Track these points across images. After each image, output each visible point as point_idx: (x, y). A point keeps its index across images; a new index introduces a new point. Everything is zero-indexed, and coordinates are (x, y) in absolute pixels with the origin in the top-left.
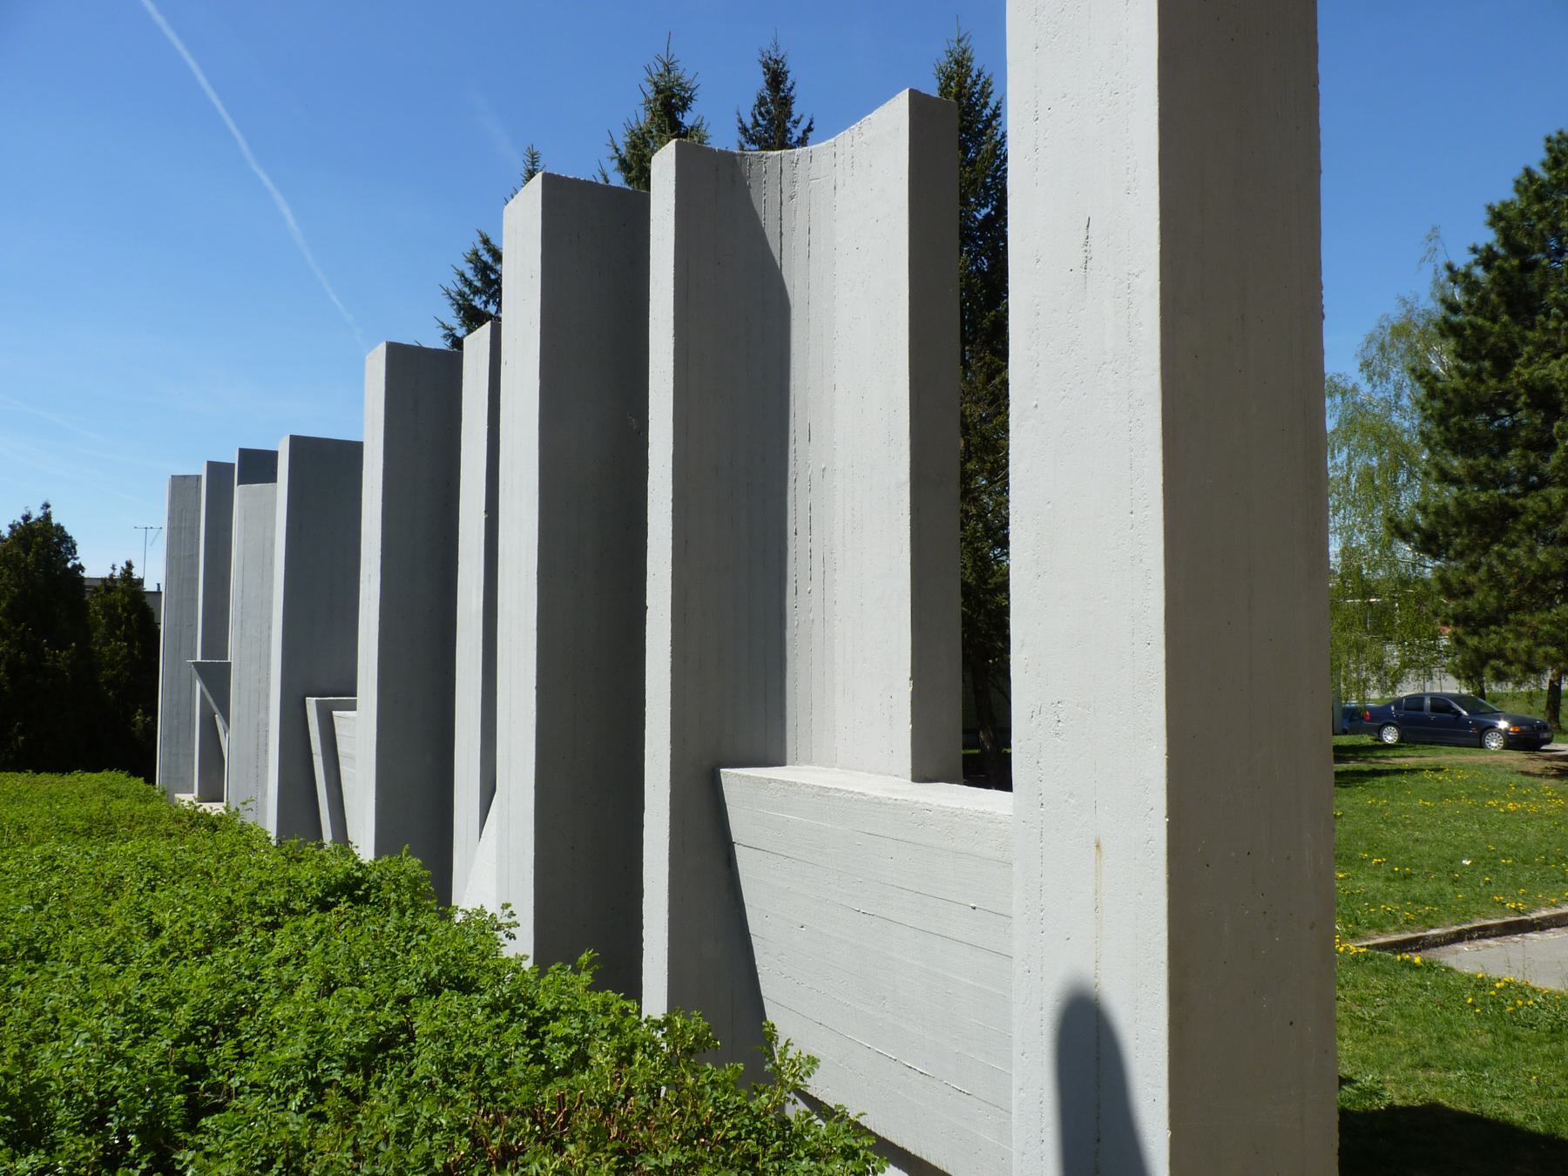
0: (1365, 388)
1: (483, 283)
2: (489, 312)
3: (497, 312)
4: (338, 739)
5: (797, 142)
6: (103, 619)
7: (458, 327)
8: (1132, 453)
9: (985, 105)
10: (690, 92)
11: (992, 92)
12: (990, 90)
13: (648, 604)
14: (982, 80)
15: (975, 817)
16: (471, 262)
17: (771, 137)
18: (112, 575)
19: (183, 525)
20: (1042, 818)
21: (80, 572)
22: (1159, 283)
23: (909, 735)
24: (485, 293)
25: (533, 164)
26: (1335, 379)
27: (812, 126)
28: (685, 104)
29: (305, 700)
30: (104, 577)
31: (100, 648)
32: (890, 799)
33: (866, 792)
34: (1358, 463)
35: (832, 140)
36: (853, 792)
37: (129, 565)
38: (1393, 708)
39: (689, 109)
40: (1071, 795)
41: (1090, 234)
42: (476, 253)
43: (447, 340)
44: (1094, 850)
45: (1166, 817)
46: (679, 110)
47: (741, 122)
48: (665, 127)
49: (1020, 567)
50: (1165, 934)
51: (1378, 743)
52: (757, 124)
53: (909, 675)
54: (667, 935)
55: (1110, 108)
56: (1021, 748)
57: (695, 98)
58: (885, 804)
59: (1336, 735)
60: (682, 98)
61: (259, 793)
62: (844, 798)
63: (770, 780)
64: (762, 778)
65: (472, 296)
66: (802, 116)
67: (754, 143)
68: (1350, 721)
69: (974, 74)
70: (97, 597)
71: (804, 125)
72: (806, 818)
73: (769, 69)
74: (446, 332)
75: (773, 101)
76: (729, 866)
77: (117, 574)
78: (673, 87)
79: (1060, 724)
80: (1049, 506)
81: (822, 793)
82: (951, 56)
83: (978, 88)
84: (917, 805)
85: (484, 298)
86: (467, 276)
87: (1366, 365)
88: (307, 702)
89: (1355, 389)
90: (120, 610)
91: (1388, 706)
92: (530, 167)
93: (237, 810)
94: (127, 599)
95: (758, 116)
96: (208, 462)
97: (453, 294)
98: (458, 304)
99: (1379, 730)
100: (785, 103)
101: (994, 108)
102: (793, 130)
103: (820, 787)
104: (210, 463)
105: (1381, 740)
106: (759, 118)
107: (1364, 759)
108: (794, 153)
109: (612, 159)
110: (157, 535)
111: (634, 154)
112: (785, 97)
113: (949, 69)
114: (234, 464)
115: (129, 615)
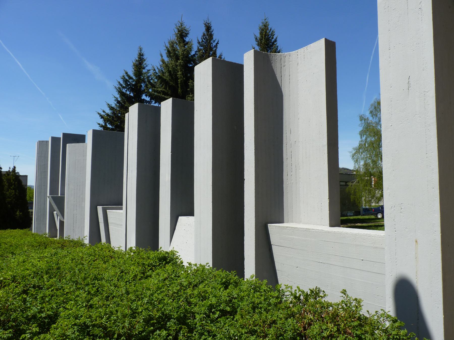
0: (371, 118)
1: (126, 85)
2: (127, 94)
3: (129, 94)
4: (109, 218)
5: (214, 47)
6: (7, 183)
7: (119, 98)
8: (426, 138)
9: (273, 38)
10: (188, 32)
11: (275, 34)
12: (274, 34)
13: (245, 178)
14: (272, 31)
15: (364, 235)
16: (122, 79)
17: (206, 45)
18: (9, 170)
19: (42, 156)
20: (396, 235)
21: (1, 169)
22: (435, 94)
23: (328, 214)
24: (126, 88)
25: (141, 51)
26: (362, 116)
27: (219, 42)
28: (186, 35)
29: (106, 212)
30: (7, 171)
31: (6, 192)
32: (332, 231)
33: (324, 230)
34: (369, 140)
35: (297, 51)
36: (319, 230)
37: (15, 167)
38: (380, 208)
39: (188, 36)
40: (406, 228)
41: (408, 80)
42: (124, 76)
43: (116, 101)
44: (415, 243)
45: (441, 233)
46: (185, 37)
47: (198, 40)
48: (181, 41)
49: (387, 168)
50: (441, 264)
51: (376, 218)
52: (203, 41)
53: (328, 198)
54: (255, 271)
55: (416, 48)
56: (388, 216)
57: (189, 33)
58: (331, 233)
59: (360, 214)
60: (186, 33)
61: (74, 235)
62: (315, 231)
63: (287, 227)
64: (284, 226)
65: (122, 89)
66: (216, 39)
67: (202, 46)
68: (365, 212)
69: (269, 29)
70: (5, 177)
71: (216, 42)
72: (300, 237)
73: (206, 26)
74: (115, 99)
75: (207, 35)
76: (270, 251)
77: (11, 170)
78: (183, 30)
79: (402, 210)
80: (397, 152)
81: (307, 230)
82: (263, 24)
83: (270, 33)
84: (343, 233)
85: (126, 89)
86: (121, 83)
87: (371, 112)
88: (98, 207)
89: (368, 119)
90: (12, 181)
91: (379, 208)
92: (140, 52)
93: (82, 239)
94: (14, 178)
95: (203, 39)
96: (52, 137)
97: (117, 88)
98: (119, 91)
99: (377, 214)
100: (211, 36)
101: (275, 39)
102: (213, 43)
103: (306, 228)
104: (52, 137)
105: (377, 217)
106: (203, 39)
107: (373, 222)
108: (284, 54)
109: (165, 50)
110: (17, 158)
111: (172, 49)
112: (211, 34)
113: (262, 27)
114: (60, 138)
115: (15, 183)
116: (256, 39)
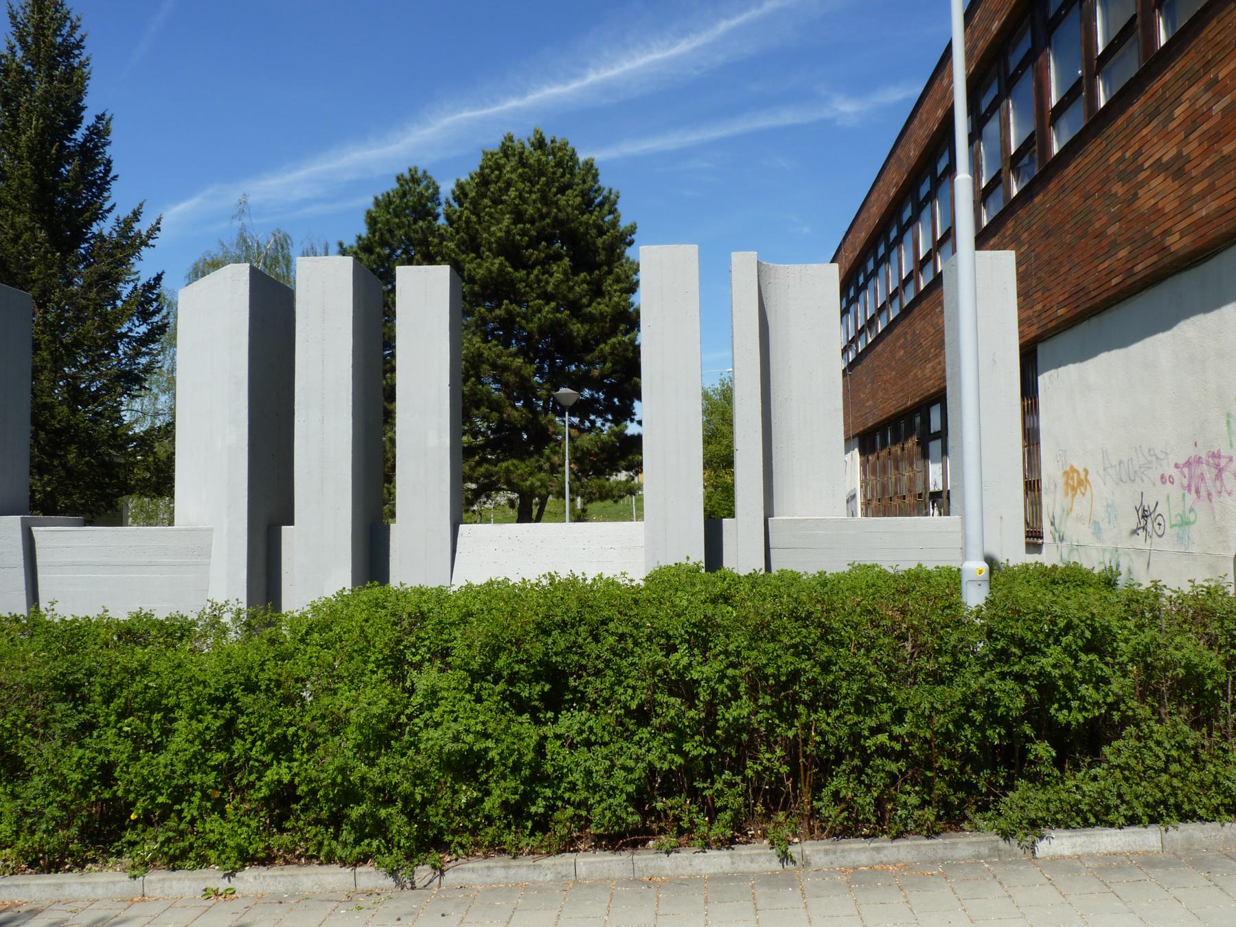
116: (13, 17)
